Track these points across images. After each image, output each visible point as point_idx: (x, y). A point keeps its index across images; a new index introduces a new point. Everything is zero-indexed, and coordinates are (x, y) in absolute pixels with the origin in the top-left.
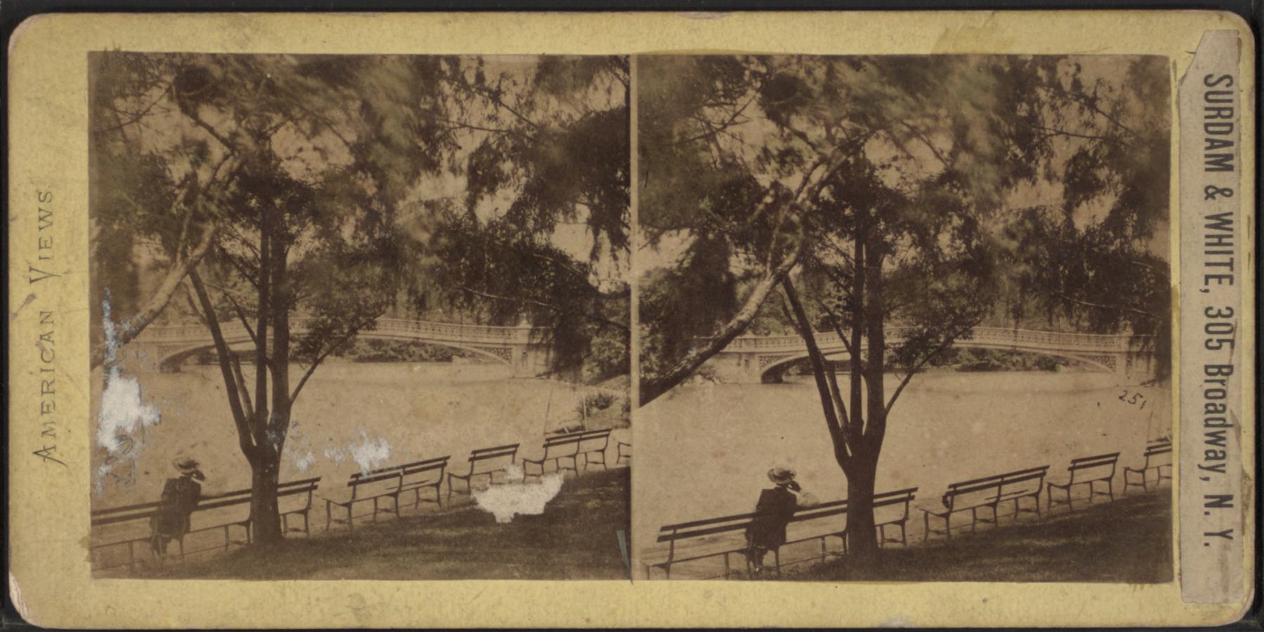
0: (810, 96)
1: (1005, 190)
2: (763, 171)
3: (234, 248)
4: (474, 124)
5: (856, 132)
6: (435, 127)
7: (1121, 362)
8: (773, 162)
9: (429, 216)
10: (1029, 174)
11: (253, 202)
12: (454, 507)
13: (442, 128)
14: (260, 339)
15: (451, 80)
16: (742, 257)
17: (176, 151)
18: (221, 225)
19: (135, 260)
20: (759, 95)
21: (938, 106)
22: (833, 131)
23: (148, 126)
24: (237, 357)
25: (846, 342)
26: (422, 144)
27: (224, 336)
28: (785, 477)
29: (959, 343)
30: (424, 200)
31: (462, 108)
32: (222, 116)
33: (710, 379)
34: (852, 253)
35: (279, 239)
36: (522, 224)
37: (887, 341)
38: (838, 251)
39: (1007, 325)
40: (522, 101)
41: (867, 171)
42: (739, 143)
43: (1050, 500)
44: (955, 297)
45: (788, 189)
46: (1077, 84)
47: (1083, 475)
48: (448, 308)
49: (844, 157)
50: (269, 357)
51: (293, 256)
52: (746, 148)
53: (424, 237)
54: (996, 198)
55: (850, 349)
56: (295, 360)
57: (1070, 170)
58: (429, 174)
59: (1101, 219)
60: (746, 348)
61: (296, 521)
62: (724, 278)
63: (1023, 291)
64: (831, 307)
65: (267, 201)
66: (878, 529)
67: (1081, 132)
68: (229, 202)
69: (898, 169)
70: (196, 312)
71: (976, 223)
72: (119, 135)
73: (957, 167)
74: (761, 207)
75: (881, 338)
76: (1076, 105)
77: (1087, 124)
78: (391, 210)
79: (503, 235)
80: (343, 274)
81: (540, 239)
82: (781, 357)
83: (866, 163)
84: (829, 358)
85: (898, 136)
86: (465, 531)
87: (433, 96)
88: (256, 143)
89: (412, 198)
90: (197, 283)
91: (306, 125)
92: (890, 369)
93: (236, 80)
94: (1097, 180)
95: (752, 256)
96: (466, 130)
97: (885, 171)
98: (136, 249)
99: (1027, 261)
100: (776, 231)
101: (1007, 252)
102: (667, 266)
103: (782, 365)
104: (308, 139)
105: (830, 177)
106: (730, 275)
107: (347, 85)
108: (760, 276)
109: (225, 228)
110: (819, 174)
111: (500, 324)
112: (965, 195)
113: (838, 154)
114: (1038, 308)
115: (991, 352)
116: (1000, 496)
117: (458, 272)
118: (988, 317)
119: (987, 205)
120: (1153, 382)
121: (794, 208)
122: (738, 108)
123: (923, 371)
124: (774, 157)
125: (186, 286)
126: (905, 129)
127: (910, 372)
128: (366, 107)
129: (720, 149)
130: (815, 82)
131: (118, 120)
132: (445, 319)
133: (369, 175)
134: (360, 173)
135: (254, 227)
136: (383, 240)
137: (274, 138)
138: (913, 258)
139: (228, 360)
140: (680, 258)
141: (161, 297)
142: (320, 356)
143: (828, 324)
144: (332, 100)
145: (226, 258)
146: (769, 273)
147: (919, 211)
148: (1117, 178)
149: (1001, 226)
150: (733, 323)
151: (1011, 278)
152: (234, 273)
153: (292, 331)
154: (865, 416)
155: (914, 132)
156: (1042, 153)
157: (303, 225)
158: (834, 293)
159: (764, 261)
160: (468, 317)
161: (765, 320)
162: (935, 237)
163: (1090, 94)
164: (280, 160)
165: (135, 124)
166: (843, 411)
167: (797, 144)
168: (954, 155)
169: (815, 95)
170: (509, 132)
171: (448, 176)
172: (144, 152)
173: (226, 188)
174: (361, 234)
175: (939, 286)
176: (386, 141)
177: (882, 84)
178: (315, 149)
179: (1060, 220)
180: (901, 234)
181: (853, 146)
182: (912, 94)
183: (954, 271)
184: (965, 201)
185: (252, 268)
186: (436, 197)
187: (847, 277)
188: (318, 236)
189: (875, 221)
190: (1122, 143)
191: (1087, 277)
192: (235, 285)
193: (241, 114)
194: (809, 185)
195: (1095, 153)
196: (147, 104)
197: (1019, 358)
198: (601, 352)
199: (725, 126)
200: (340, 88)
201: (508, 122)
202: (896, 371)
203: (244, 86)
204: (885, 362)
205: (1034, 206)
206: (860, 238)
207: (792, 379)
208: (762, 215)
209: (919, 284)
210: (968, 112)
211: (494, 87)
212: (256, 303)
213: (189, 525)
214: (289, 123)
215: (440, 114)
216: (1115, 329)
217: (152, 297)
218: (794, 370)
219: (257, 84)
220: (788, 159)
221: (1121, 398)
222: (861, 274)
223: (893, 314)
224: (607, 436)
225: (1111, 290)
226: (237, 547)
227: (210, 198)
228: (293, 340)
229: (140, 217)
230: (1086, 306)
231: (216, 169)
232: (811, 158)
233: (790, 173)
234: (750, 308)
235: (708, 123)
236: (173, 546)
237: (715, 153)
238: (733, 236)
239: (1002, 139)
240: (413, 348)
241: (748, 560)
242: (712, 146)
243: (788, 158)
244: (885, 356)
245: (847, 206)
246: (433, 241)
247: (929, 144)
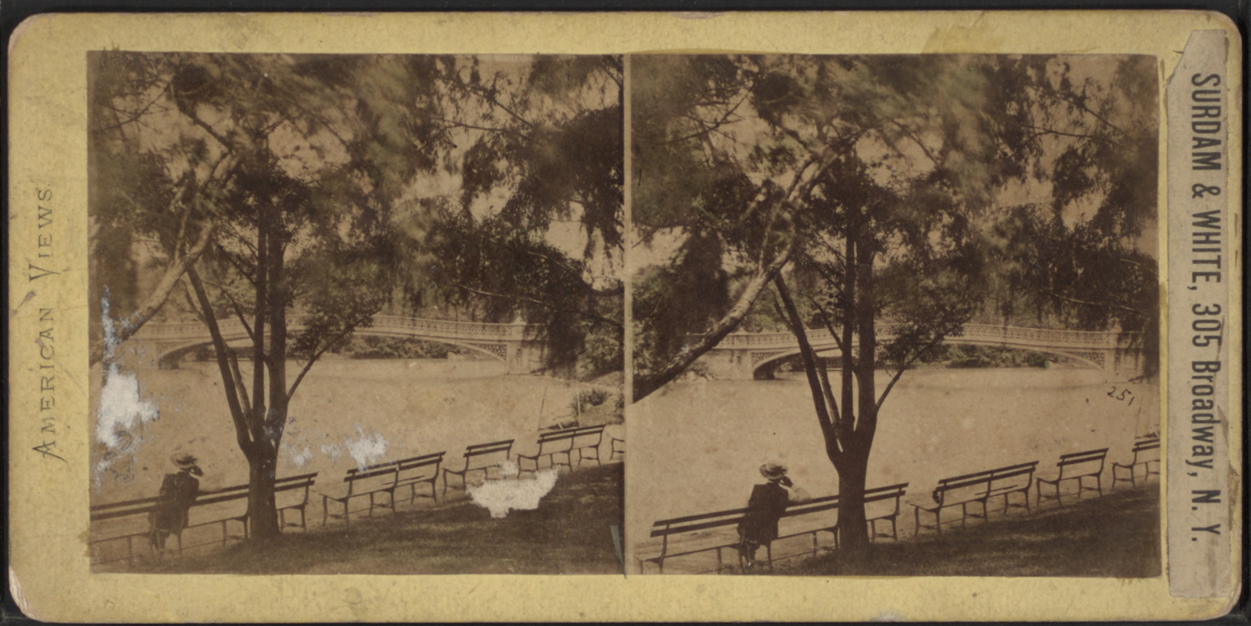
0: (802, 95)
1: (994, 188)
2: (755, 169)
3: (231, 246)
4: (470, 123)
5: (847, 131)
6: (432, 126)
7: (1109, 359)
8: (765, 160)
9: (425, 214)
10: (1018, 172)
11: (251, 200)
12: (452, 502)
13: (438, 127)
14: (257, 336)
15: (446, 80)
16: (735, 254)
17: (174, 150)
18: (219, 223)
19: (134, 257)
20: (751, 94)
21: (929, 105)
22: (825, 129)
23: (146, 125)
24: (235, 354)
25: (837, 339)
26: (417, 143)
27: (222, 332)
28: (777, 472)
29: (949, 340)
30: (420, 198)
31: (457, 107)
32: (220, 115)
33: (703, 375)
34: (843, 251)
35: (276, 237)
36: (516, 222)
37: (877, 338)
38: (830, 249)
39: (997, 322)
40: (517, 101)
41: (858, 169)
42: (731, 142)
43: (1039, 495)
44: (945, 294)
45: (780, 188)
46: (1066, 83)
47: (1071, 471)
48: (443, 305)
49: (835, 156)
50: (267, 353)
51: (290, 254)
52: (738, 147)
53: (420, 235)
54: (986, 196)
55: (841, 346)
56: (292, 356)
57: (1059, 168)
58: (425, 172)
59: (1089, 217)
60: (738, 345)
61: (293, 516)
62: (717, 275)
63: (1013, 288)
64: (823, 304)
65: (264, 199)
66: (869, 524)
67: (1070, 131)
68: (227, 200)
69: (889, 167)
70: (194, 309)
71: (966, 221)
72: (118, 133)
73: (947, 165)
74: (753, 205)
75: (872, 334)
76: (1065, 104)
77: (1076, 123)
78: (387, 208)
79: (498, 233)
80: (339, 271)
81: (534, 237)
82: (773, 354)
83: (857, 161)
84: (820, 355)
85: (889, 134)
86: (460, 526)
87: (429, 95)
88: (254, 141)
89: (408, 196)
90: (195, 281)
91: (303, 124)
92: (881, 365)
93: (234, 79)
94: (1086, 178)
95: (745, 254)
96: (461, 129)
97: (876, 170)
98: (134, 246)
99: (1016, 259)
100: (768, 229)
101: (997, 249)
102: (660, 264)
103: (774, 361)
104: (305, 137)
105: (821, 175)
106: (723, 273)
107: (343, 84)
108: (752, 274)
109: (223, 226)
110: (810, 173)
111: (495, 321)
112: (955, 193)
113: (829, 152)
114: (1027, 305)
115: (981, 349)
116: (989, 491)
117: (454, 269)
118: (978, 314)
119: (977, 204)
120: (1141, 378)
121: (786, 206)
122: (731, 107)
123: (914, 367)
124: (766, 156)
125: (184, 283)
126: (896, 128)
127: (901, 369)
128: (362, 106)
129: (712, 148)
130: (807, 81)
131: (117, 118)
132: (440, 315)
133: (366, 174)
134: (356, 172)
135: (251, 225)
136: (379, 238)
137: (271, 137)
138: (904, 256)
139: (226, 357)
140: (673, 256)
141: (160, 294)
142: (317, 352)
143: (817, 322)
144: (329, 99)
145: (224, 256)
146: (761, 270)
147: (909, 209)
148: (1106, 176)
149: (991, 224)
150: (726, 320)
151: (1001, 276)
152: (232, 270)
153: (289, 328)
154: (856, 412)
155: (904, 131)
156: (1031, 151)
157: (300, 223)
158: (825, 290)
159: (756, 259)
160: (463, 314)
161: (757, 317)
162: (926, 234)
163: (1079, 93)
164: (277, 159)
165: (134, 123)
166: (834, 407)
167: (789, 142)
168: (944, 153)
169: (807, 94)
170: (504, 131)
171: (443, 174)
172: (143, 151)
173: (224, 186)
174: (358, 232)
175: (930, 283)
176: (382, 140)
177: (873, 83)
178: (312, 147)
179: (1049, 218)
180: (891, 231)
181: (844, 144)
182: (903, 93)
183: (944, 268)
184: (955, 199)
185: (250, 265)
186: (431, 195)
187: (839, 274)
188: (315, 234)
189: (866, 219)
190: (1111, 142)
191: (1076, 274)
192: (232, 282)
193: (238, 113)
194: (801, 184)
195: (1084, 151)
196: (146, 104)
197: (1008, 355)
198: (595, 348)
199: (718, 125)
200: (337, 87)
201: (503, 121)
202: (887, 368)
203: (242, 85)
204: (876, 359)
205: (1023, 204)
206: (851, 236)
207: (784, 375)
208: (754, 213)
209: (910, 281)
210: (958, 111)
211: (489, 86)
212: (254, 300)
213: (187, 520)
214: (286, 122)
215: (435, 113)
216: (1103, 326)
217: (150, 295)
218: (785, 367)
219: (254, 83)
220: (780, 158)
221: (1109, 394)
222: (853, 272)
223: (883, 311)
224: (601, 432)
225: (1100, 288)
226: (234, 542)
227: (208, 197)
228: (290, 337)
229: (138, 215)
230: (483, 296)
231: (214, 168)
232: (802, 157)
233: (781, 172)
234: (743, 305)
235: (701, 122)
236: (171, 541)
237: (708, 151)
238: (725, 233)
239: (992, 138)
240: (408, 345)
241: (741, 555)
242: (705, 145)
243: (780, 156)
244: (876, 352)
245: (838, 205)
246: (429, 238)
247: (920, 143)
